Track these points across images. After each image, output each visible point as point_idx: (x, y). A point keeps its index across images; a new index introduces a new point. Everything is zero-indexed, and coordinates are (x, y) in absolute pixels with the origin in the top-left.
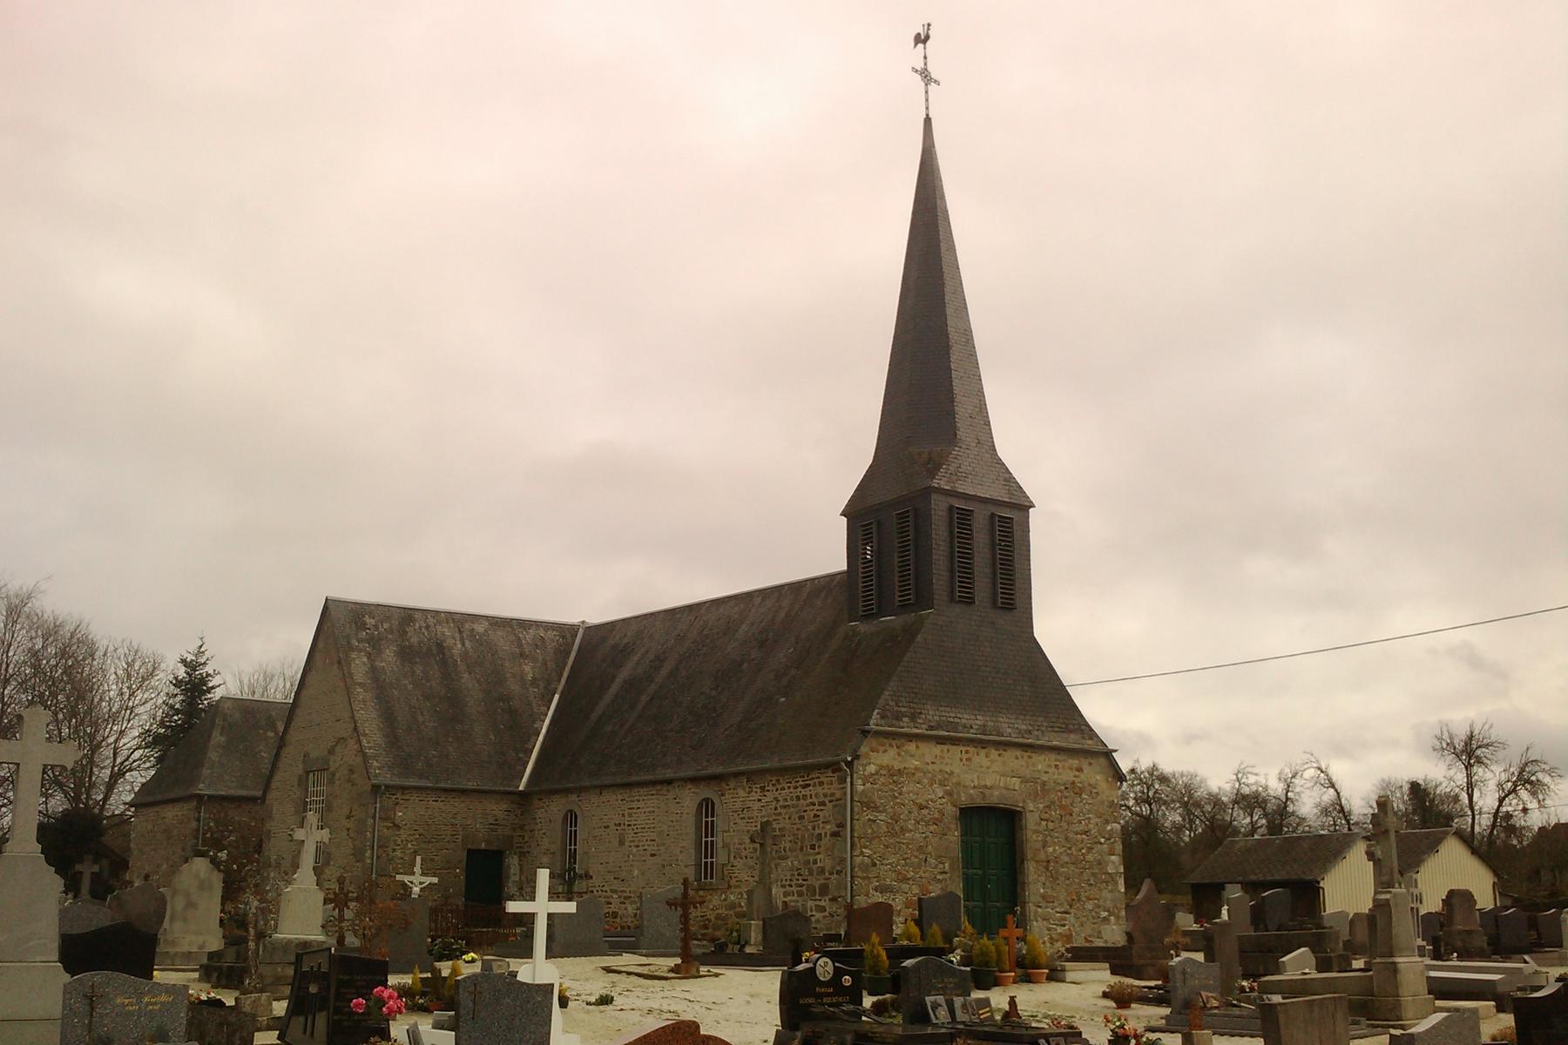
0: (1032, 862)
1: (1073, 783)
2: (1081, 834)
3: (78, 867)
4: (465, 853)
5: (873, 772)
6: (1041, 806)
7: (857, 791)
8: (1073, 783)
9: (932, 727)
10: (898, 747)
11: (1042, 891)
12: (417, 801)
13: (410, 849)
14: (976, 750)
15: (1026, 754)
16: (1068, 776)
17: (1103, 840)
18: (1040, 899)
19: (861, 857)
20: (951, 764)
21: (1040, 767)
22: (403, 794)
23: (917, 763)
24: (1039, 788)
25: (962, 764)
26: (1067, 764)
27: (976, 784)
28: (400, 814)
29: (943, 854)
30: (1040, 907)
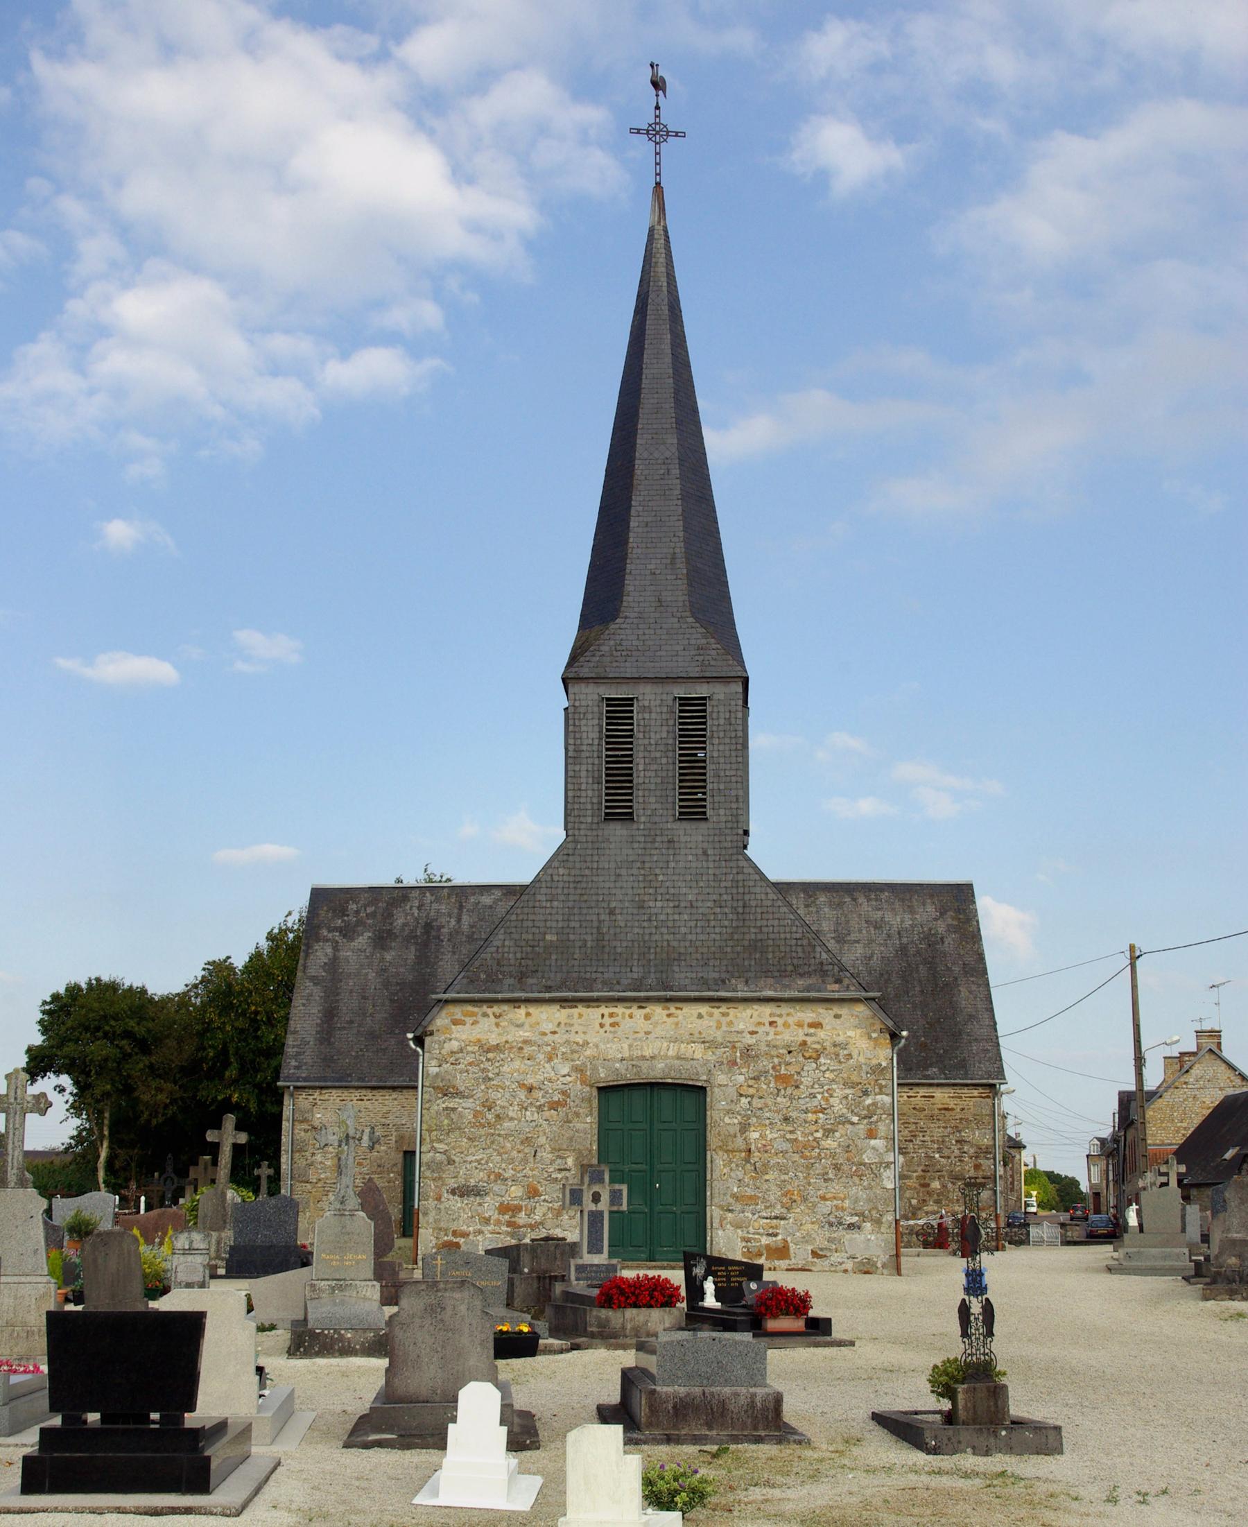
0: (721, 1153)
1: (804, 1043)
2: (815, 1112)
3: (256, 1172)
4: (401, 1155)
5: (455, 1050)
6: (741, 1078)
7: (428, 1075)
8: (804, 1043)
9: (550, 987)
10: (496, 1017)
11: (735, 1190)
12: (338, 1101)
13: (332, 1153)
14: (628, 1012)
15: (716, 1011)
16: (792, 1035)
17: (855, 1119)
18: (731, 1200)
19: (431, 1154)
20: (584, 1033)
21: (741, 1026)
22: (321, 1094)
23: (526, 1034)
24: (738, 1054)
25: (602, 1031)
26: (791, 1020)
27: (626, 1055)
28: (319, 1116)
29: (565, 1147)
30: (731, 1211)
